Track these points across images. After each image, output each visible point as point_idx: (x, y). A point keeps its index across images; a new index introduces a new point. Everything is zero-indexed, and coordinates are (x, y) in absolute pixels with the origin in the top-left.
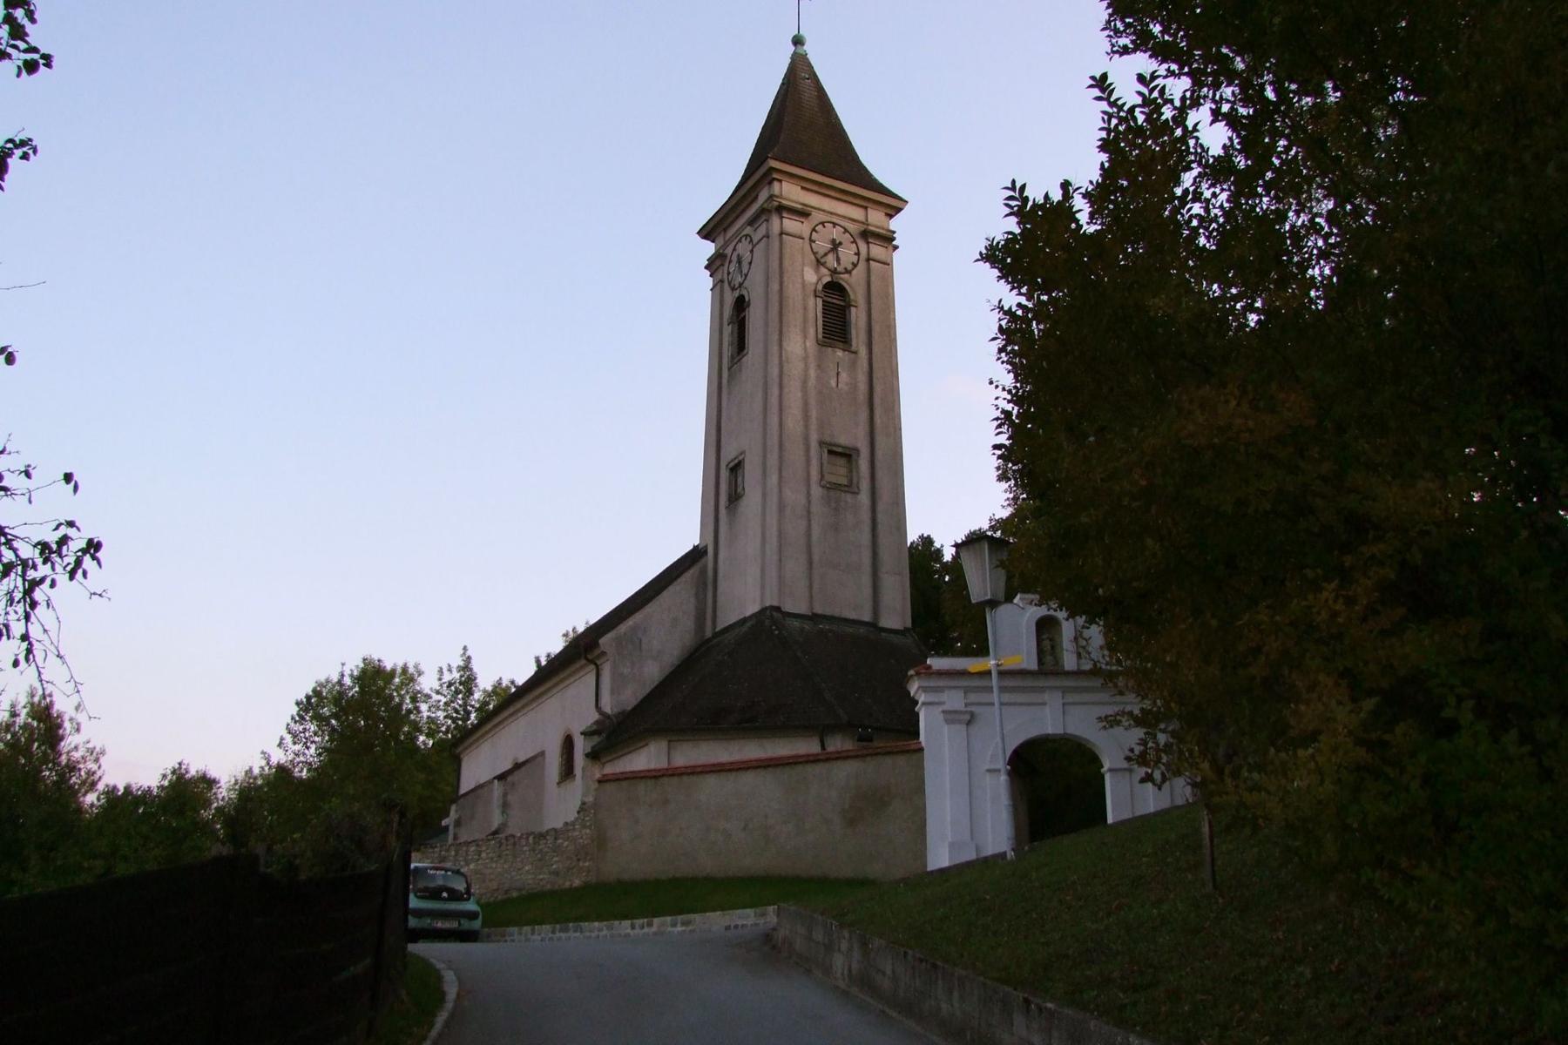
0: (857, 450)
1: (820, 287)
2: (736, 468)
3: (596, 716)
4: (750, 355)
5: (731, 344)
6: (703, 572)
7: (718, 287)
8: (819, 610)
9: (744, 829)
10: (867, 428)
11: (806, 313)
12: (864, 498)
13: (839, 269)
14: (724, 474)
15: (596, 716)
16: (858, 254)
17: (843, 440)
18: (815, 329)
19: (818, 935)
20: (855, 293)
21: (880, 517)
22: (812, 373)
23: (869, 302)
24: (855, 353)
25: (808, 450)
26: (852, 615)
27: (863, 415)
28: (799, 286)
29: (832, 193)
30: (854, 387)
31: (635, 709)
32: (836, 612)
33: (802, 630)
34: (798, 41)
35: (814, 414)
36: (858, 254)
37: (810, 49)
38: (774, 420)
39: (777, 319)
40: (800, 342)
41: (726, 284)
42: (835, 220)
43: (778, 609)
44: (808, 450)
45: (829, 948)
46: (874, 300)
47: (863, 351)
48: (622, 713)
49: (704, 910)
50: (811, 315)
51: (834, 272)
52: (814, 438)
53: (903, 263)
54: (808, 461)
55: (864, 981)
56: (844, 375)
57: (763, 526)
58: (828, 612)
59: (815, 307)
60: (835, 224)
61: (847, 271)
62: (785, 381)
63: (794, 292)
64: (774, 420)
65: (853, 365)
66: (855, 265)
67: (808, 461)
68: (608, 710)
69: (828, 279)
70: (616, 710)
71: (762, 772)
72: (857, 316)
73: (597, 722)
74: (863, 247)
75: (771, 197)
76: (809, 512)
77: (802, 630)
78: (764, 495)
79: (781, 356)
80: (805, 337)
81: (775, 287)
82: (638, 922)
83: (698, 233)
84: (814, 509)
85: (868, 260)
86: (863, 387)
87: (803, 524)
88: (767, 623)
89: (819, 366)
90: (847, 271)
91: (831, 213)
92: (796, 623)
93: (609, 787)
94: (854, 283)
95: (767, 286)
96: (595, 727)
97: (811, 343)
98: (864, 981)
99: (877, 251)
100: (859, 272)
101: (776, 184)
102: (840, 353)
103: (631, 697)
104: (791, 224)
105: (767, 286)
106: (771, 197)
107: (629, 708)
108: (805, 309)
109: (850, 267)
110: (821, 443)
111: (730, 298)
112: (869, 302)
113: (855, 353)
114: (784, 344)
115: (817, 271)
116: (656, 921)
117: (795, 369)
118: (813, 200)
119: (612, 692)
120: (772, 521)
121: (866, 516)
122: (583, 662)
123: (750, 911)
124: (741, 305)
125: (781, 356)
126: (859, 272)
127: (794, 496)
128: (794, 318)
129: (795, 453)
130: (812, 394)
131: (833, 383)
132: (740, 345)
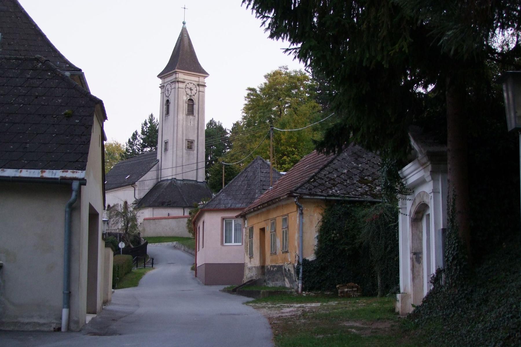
0: (194, 140)
1: (187, 100)
2: (166, 143)
3: (134, 199)
4: (170, 116)
5: (165, 111)
6: (158, 166)
7: (162, 93)
8: (184, 178)
9: (170, 228)
10: (197, 135)
11: (184, 107)
12: (195, 152)
13: (192, 95)
14: (164, 144)
15: (134, 199)
16: (197, 90)
17: (191, 138)
18: (185, 111)
19: (180, 246)
20: (195, 100)
21: (199, 156)
22: (184, 123)
23: (199, 103)
24: (195, 116)
25: (183, 141)
26: (192, 179)
27: (196, 132)
28: (182, 101)
29: (191, 75)
30: (194, 125)
31: (143, 198)
32: (188, 179)
33: (180, 183)
34: (184, 23)
35: (184, 132)
36: (197, 90)
37: (187, 25)
38: (175, 135)
39: (177, 110)
40: (182, 115)
41: (164, 94)
42: (191, 82)
43: (175, 179)
44: (183, 141)
45: (181, 247)
46: (200, 102)
47: (197, 116)
48: (141, 199)
49: (163, 242)
50: (185, 108)
51: (191, 96)
52: (184, 138)
53: (207, 90)
54: (183, 144)
55: (184, 250)
56: (192, 122)
57: (173, 160)
58: (186, 179)
59: (186, 106)
60: (191, 83)
61: (194, 95)
62: (178, 126)
63: (181, 103)
64: (175, 135)
65: (194, 119)
66: (196, 93)
67: (183, 144)
68: (137, 198)
69: (189, 98)
70: (139, 198)
71: (173, 219)
72: (196, 107)
73: (135, 201)
74: (198, 88)
75: (176, 78)
76: (183, 156)
77: (180, 183)
78: (173, 152)
79: (177, 119)
80: (183, 114)
81: (176, 102)
82: (153, 244)
83: (158, 76)
84: (184, 155)
85: (199, 92)
86: (196, 125)
87: (181, 159)
88: (173, 182)
89: (186, 121)
90: (194, 95)
91: (190, 80)
92: (179, 182)
93: (146, 221)
94: (195, 99)
95: (175, 101)
96: (135, 202)
97: (184, 115)
98: (184, 250)
99: (201, 89)
100: (196, 95)
101: (177, 74)
102: (191, 117)
103: (142, 195)
104: (181, 85)
105: (175, 101)
106: (176, 78)
107: (142, 198)
108: (183, 107)
109: (194, 94)
110: (186, 140)
111: (166, 99)
112: (199, 103)
113: (195, 116)
114: (178, 117)
115: (186, 96)
116: (156, 244)
117: (180, 123)
118: (186, 77)
119: (138, 194)
120: (175, 158)
121: (196, 156)
122: (131, 186)
123: (171, 242)
124: (168, 101)
125: (177, 119)
126: (196, 95)
127: (180, 153)
128: (181, 109)
129: (180, 142)
130: (184, 128)
131: (189, 125)
132: (168, 113)
